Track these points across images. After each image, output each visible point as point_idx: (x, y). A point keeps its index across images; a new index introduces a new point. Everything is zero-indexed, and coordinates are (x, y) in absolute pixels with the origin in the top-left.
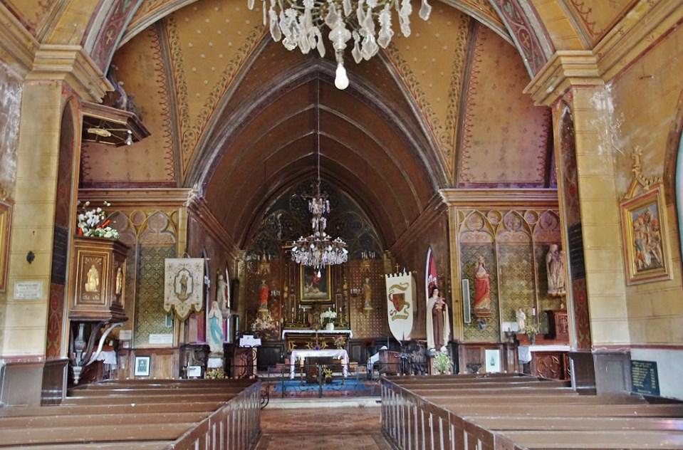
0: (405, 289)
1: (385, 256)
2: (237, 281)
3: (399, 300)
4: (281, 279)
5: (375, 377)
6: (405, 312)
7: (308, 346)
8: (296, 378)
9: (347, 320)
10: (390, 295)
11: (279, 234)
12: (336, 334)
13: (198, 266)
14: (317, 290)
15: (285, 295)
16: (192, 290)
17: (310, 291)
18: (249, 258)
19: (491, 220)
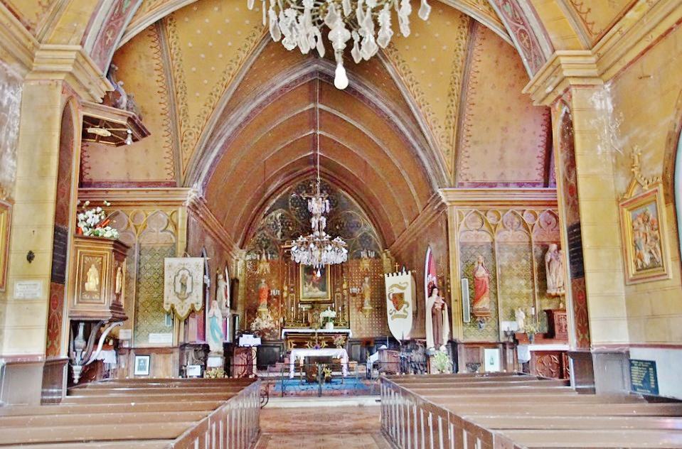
0: (404, 288)
2: (238, 281)
6: (404, 311)
7: (307, 345)
8: (296, 377)
9: (346, 319)
11: (279, 234)
14: (317, 289)
15: (285, 294)
17: (309, 290)
18: (249, 257)
19: (491, 219)
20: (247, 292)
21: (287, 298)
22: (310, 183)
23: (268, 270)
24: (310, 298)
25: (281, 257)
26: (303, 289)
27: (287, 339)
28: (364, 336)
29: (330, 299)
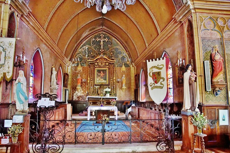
0: (161, 69)
1: (131, 66)
2: (67, 75)
3: (157, 76)
4: (87, 74)
5: (129, 119)
6: (161, 84)
7: (98, 103)
8: (91, 120)
9: (115, 93)
10: (150, 73)
11: (87, 55)
12: (110, 98)
13: (10, 44)
14: (102, 79)
15: (89, 81)
16: (5, 61)
17: (99, 80)
18: (73, 65)
19: (220, 22)
20: (72, 80)
21: (89, 83)
22: (100, 34)
23: (82, 70)
24: (99, 83)
25: (87, 65)
26: (96, 79)
27: (89, 101)
28: (122, 100)
29: (108, 84)
